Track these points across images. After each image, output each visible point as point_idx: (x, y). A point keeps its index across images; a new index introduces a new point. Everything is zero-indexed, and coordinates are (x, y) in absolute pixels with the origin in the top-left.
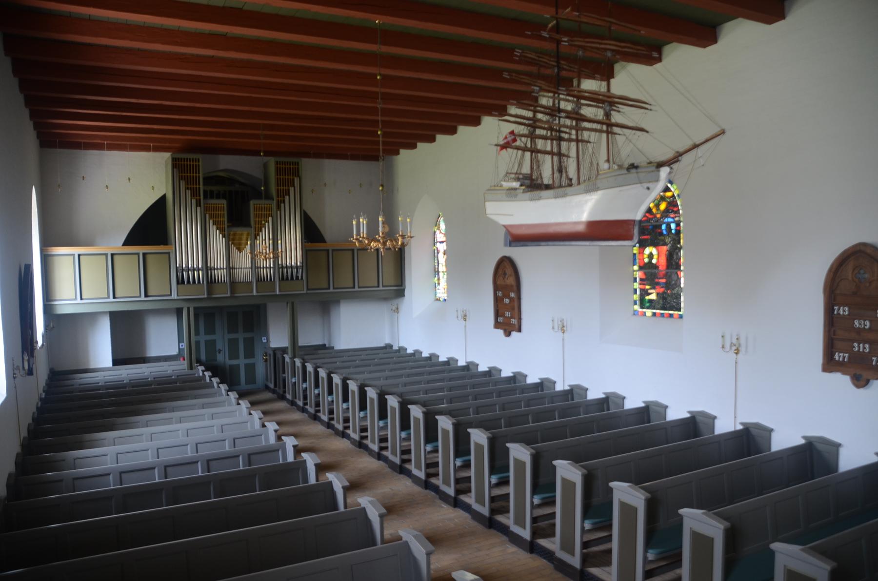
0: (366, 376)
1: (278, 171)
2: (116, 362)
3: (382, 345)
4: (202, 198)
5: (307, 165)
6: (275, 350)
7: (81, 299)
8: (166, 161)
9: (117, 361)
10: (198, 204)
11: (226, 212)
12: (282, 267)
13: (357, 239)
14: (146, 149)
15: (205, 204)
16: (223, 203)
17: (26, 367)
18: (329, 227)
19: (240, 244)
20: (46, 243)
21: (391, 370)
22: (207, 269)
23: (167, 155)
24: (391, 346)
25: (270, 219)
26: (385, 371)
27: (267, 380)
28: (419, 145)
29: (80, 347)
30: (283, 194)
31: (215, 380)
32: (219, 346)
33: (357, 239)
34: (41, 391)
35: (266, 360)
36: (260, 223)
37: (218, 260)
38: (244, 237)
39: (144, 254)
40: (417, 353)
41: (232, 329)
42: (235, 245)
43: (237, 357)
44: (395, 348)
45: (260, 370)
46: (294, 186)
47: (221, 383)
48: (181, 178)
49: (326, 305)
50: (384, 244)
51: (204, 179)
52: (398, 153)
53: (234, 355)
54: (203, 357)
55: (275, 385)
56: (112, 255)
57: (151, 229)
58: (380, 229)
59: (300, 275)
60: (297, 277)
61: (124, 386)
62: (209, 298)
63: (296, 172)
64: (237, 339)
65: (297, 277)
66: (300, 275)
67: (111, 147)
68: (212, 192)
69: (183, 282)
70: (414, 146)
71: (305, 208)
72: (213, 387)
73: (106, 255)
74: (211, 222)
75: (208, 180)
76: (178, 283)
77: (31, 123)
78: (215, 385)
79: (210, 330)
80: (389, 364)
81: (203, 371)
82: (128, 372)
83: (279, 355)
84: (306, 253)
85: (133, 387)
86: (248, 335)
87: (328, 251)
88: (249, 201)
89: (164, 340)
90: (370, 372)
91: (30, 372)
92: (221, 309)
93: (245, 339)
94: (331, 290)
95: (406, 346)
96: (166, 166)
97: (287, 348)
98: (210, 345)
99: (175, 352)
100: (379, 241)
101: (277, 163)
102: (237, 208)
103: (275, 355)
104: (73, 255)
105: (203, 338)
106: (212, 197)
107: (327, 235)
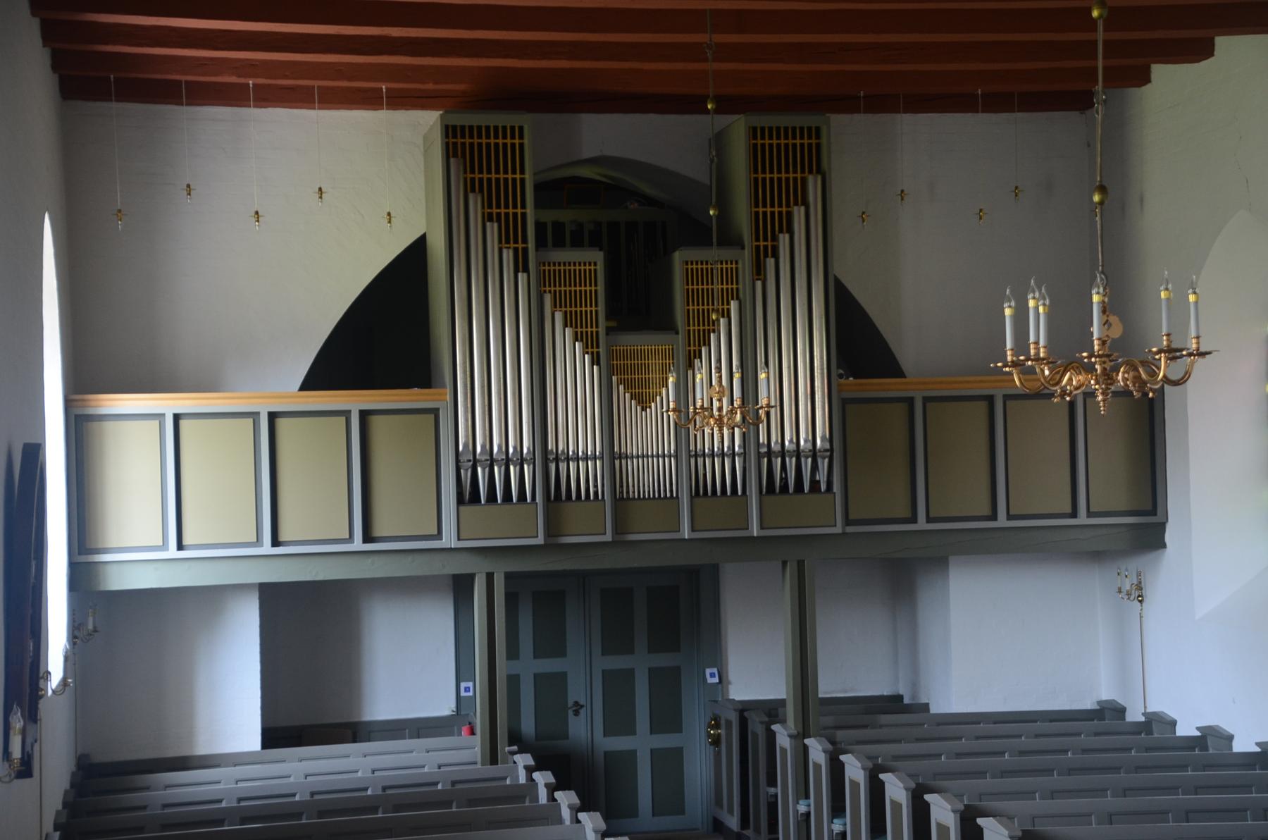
0: (1037, 805)
1: (757, 158)
2: (274, 737)
3: (1088, 704)
4: (531, 245)
5: (847, 133)
6: (745, 709)
7: (180, 547)
8: (425, 138)
9: (276, 735)
10: (521, 264)
11: (601, 288)
12: (770, 453)
13: (1015, 364)
14: (369, 100)
15: (541, 263)
16: (597, 258)
17: (16, 752)
18: (919, 325)
19: (644, 383)
20: (81, 382)
21: (1125, 792)
22: (547, 457)
23: (430, 119)
24: (1120, 711)
25: (734, 305)
26: (1101, 792)
27: (719, 803)
28: (1221, 42)
29: (171, 691)
30: (772, 228)
31: (566, 799)
32: (576, 692)
33: (1015, 364)
34: (49, 826)
35: (716, 741)
36: (704, 318)
37: (578, 432)
38: (655, 362)
39: (364, 415)
40: (1211, 738)
41: (616, 641)
42: (628, 385)
43: (630, 730)
44: (1135, 715)
45: (699, 769)
46: (805, 203)
47: (584, 807)
48: (470, 187)
49: (901, 572)
50: (1108, 377)
51: (538, 187)
52: (1145, 79)
53: (618, 721)
54: (528, 726)
55: (745, 822)
56: (273, 416)
57: (382, 341)
58: (1095, 329)
59: (822, 477)
60: (815, 485)
61: (294, 812)
62: (551, 547)
63: (814, 161)
64: (629, 675)
65: (815, 485)
66: (822, 477)
67: (268, 97)
68: (558, 226)
69: (475, 498)
70: (1202, 50)
71: (837, 270)
72: (560, 821)
73: (255, 415)
74: (559, 316)
75: (549, 191)
76: (460, 501)
77: (35, 24)
78: (566, 813)
79: (551, 644)
80: (1116, 769)
81: (530, 770)
82: (308, 769)
83: (756, 726)
84: (841, 407)
85: (321, 814)
86: (663, 660)
87: (910, 401)
88: (668, 253)
89: (414, 669)
90: (1053, 794)
91: (25, 769)
92: (582, 578)
93: (653, 673)
94: (922, 524)
95: (1172, 713)
96: (426, 152)
97: (782, 703)
98: (552, 687)
99: (445, 707)
100: (1090, 369)
101: (753, 132)
102: (632, 269)
103: (743, 723)
104: (160, 416)
105: (530, 666)
106: (559, 243)
107: (907, 352)
